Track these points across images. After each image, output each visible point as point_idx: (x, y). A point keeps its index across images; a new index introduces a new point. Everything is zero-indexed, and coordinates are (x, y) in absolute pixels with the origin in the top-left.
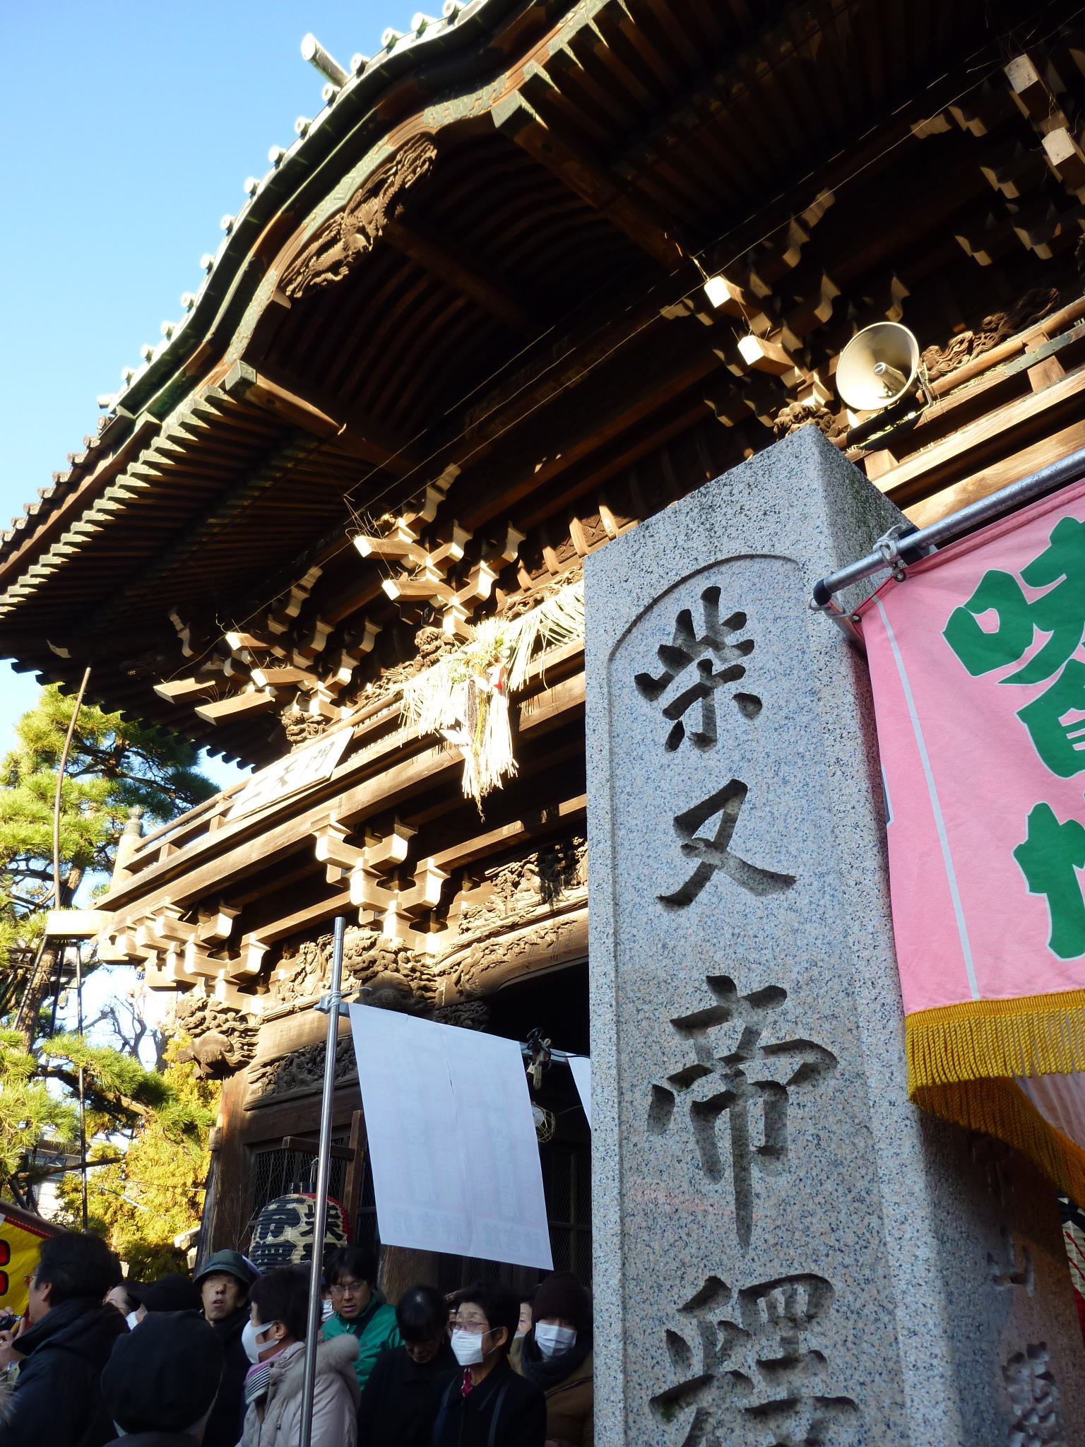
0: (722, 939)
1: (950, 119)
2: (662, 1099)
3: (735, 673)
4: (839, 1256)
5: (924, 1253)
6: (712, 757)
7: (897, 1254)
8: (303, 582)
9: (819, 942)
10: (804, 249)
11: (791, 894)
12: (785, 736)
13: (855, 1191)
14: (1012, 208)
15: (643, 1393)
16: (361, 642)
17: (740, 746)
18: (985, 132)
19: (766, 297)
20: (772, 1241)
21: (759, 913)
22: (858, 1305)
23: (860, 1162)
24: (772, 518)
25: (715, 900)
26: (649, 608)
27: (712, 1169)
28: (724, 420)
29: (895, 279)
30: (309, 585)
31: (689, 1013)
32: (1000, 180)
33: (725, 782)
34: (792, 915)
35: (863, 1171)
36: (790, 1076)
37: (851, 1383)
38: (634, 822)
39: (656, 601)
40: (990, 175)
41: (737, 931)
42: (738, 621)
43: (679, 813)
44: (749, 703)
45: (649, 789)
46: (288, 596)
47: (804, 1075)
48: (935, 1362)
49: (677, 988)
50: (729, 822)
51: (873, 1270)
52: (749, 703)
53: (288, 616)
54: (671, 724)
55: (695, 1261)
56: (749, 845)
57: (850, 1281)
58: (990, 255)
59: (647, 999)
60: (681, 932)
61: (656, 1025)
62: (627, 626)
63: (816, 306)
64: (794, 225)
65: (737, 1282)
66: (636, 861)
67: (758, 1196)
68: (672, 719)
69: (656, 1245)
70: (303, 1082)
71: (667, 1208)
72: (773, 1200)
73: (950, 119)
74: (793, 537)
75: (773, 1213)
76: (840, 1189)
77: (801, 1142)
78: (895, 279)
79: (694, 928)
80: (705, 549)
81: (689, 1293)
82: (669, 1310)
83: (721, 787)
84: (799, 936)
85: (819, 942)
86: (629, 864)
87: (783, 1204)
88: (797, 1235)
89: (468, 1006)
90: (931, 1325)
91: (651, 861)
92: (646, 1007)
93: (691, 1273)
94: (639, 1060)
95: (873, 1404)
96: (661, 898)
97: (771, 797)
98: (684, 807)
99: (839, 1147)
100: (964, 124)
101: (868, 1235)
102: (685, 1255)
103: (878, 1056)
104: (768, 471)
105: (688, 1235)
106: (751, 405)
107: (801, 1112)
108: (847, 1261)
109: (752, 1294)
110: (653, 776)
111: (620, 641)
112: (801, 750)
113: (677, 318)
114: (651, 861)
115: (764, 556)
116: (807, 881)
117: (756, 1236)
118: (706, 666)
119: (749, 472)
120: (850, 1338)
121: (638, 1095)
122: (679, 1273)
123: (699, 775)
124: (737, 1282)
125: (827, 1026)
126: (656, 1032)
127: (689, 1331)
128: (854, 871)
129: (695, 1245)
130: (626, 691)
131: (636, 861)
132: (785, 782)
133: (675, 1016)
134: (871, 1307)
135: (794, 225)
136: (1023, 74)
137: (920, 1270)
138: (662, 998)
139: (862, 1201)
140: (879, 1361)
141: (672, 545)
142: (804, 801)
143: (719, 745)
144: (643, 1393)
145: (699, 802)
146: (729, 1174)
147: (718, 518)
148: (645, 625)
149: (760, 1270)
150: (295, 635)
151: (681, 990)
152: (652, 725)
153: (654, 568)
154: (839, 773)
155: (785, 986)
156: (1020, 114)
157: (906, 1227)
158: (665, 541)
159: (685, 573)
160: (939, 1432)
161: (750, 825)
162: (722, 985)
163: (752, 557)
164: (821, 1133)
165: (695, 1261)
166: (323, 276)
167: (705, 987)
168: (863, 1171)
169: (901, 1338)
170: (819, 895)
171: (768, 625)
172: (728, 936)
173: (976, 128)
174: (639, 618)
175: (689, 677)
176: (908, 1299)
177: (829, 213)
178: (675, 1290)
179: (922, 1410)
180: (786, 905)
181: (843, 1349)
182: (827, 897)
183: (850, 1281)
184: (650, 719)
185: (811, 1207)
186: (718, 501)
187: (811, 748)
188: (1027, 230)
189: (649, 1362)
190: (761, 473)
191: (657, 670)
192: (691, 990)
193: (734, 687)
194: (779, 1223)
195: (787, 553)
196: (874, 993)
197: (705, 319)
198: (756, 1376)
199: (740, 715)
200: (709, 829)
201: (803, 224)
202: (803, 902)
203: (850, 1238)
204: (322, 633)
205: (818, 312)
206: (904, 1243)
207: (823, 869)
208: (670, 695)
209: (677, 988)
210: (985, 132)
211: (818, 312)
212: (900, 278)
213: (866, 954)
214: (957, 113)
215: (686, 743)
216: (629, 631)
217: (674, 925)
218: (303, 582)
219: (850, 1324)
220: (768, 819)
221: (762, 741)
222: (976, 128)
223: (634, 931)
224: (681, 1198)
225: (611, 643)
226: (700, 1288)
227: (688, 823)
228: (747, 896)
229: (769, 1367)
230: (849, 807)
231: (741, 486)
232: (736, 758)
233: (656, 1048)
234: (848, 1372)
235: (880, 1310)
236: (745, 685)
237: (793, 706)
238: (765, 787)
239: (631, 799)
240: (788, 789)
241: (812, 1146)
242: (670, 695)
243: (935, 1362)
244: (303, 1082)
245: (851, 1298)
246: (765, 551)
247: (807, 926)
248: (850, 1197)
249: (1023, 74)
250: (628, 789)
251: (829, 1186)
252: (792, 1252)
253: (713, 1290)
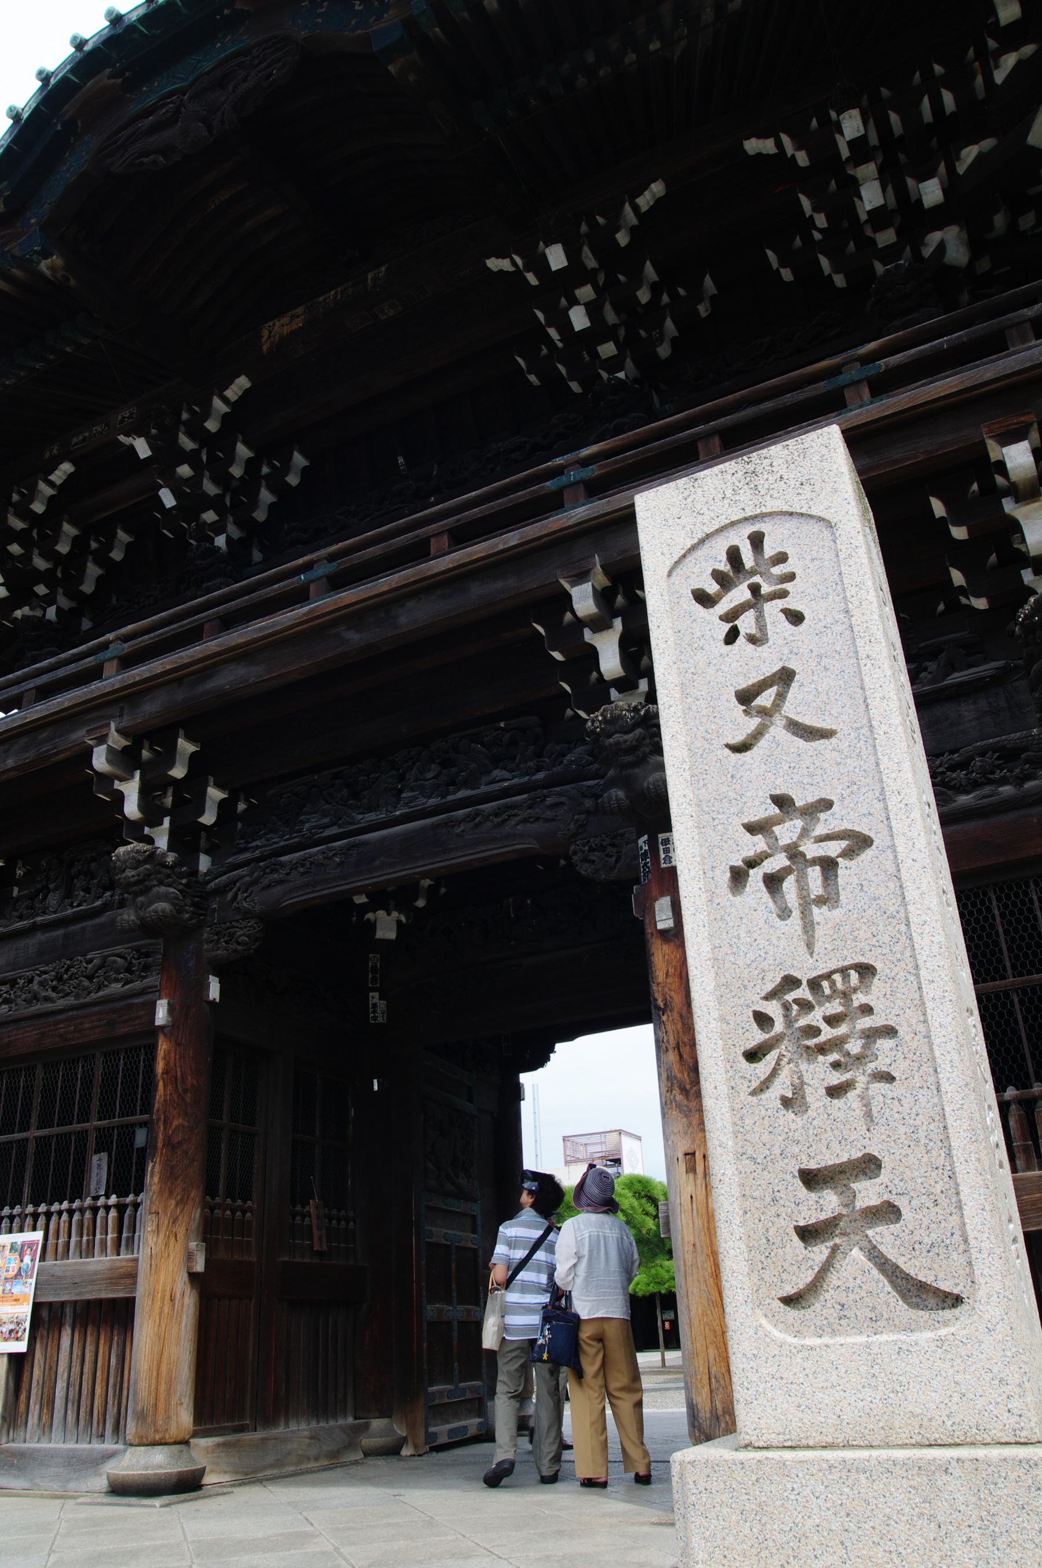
0: (781, 771)
1: (779, 144)
2: (738, 877)
3: (783, 594)
4: (879, 950)
5: (940, 938)
6: (763, 650)
7: (920, 942)
8: (52, 477)
9: (857, 770)
10: (633, 231)
11: (833, 740)
12: (825, 639)
13: (888, 913)
14: (817, 236)
15: (737, 1050)
16: (111, 550)
17: (783, 646)
18: (808, 164)
19: (593, 269)
20: (830, 948)
21: (810, 753)
22: (893, 974)
23: (892, 896)
24: (807, 488)
25: (774, 745)
26: (702, 541)
27: (784, 913)
28: (532, 378)
29: (648, 262)
30: (59, 482)
31: (757, 818)
32: (816, 209)
33: (776, 668)
34: (835, 753)
35: (894, 901)
36: (839, 851)
37: (890, 1016)
38: (699, 693)
39: (708, 536)
40: (805, 202)
41: (792, 765)
42: (781, 558)
43: (740, 688)
44: (795, 618)
45: (711, 670)
46: (33, 489)
47: (848, 854)
48: (946, 994)
49: (745, 803)
50: (781, 697)
51: (902, 953)
52: (795, 618)
53: (32, 511)
54: (727, 627)
55: (772, 967)
56: (799, 710)
57: (887, 962)
58: (794, 273)
59: (721, 811)
60: (746, 767)
61: (730, 828)
62: (683, 552)
63: (639, 289)
64: (627, 208)
65: (804, 976)
66: (704, 720)
67: (818, 924)
68: (728, 622)
69: (740, 963)
70: (47, 999)
71: (748, 939)
72: (830, 925)
73: (779, 144)
74: (826, 504)
75: (831, 932)
76: (878, 913)
77: (849, 888)
78: (648, 262)
79: (758, 763)
80: (751, 503)
81: (770, 987)
82: (754, 999)
83: (774, 670)
84: (841, 766)
85: (857, 770)
86: (697, 722)
87: (837, 927)
88: (849, 942)
89: (244, 924)
90: (943, 976)
91: (717, 720)
92: (720, 816)
93: (769, 976)
94: (716, 851)
95: (905, 1024)
96: (728, 746)
97: (815, 678)
98: (743, 684)
99: (877, 889)
100: (790, 150)
101: (898, 936)
102: (765, 965)
103: (904, 834)
104: (804, 453)
105: (766, 953)
106: (562, 369)
107: (848, 872)
108: (884, 951)
109: (814, 985)
110: (714, 661)
111: (677, 563)
112: (838, 649)
113: (501, 271)
114: (717, 720)
115: (802, 514)
116: (846, 733)
117: (818, 947)
118: (755, 589)
119: (786, 452)
120: (889, 993)
121: (718, 872)
122: (760, 976)
123: (751, 664)
124: (804, 976)
125: (865, 820)
126: (730, 832)
127: (773, 1008)
128: (883, 726)
129: (771, 958)
130: (683, 600)
131: (704, 720)
132: (826, 669)
133: (746, 821)
134: (902, 974)
135: (627, 208)
136: (852, 125)
137: (935, 949)
138: (734, 810)
139: (894, 917)
140: (909, 1001)
141: (721, 496)
142: (841, 682)
143: (770, 643)
144: (737, 1050)
145: (756, 680)
146: (796, 913)
147: (760, 481)
148: (699, 553)
149: (822, 966)
150: (35, 534)
151: (749, 804)
152: (710, 626)
153: (705, 510)
154: (869, 665)
155: (833, 798)
156: (839, 155)
157: (926, 927)
158: (713, 492)
159: (735, 518)
160: (950, 1029)
161: (800, 697)
162: (782, 802)
163: (791, 514)
164: (864, 883)
165: (772, 967)
166: (152, 157)
167: (769, 801)
168: (894, 901)
169: (923, 986)
170: (855, 741)
171: (807, 562)
172: (786, 767)
173: (802, 159)
174: (693, 548)
175: (741, 594)
176: (928, 965)
177: (659, 202)
178: (758, 986)
179: (939, 1020)
180: (830, 747)
181: (883, 1000)
182: (862, 742)
183: (887, 962)
184: (711, 622)
185: (857, 925)
186: (759, 469)
187: (846, 648)
188: (829, 259)
189: (740, 1031)
190: (796, 454)
191: (712, 588)
192: (757, 804)
193: (780, 604)
194: (835, 937)
195: (822, 515)
196: (900, 798)
197: (532, 279)
198: (823, 1026)
199: (787, 623)
200: (766, 699)
201: (636, 208)
202: (844, 745)
203: (886, 939)
204: (67, 535)
205: (639, 293)
206: (924, 935)
207: (859, 725)
208: (725, 605)
209: (745, 803)
210: (808, 164)
211: (639, 293)
212: (711, 276)
213: (894, 775)
214: (786, 139)
215: (741, 640)
216: (684, 556)
217: (740, 763)
218: (52, 477)
219: (888, 985)
220: (814, 692)
221: (806, 642)
222: (802, 159)
223: (707, 767)
224: (759, 932)
225: (669, 564)
226: (776, 983)
227: (745, 697)
228: (801, 742)
229: (832, 1021)
230: (878, 686)
231: (780, 461)
232: (786, 652)
233: (730, 842)
234: (888, 1011)
235: (908, 975)
236: (791, 603)
237: (829, 620)
238: (810, 672)
239: (695, 677)
240: (828, 674)
241: (857, 891)
242: (725, 605)
243: (946, 994)
244: (47, 999)
245: (888, 971)
246: (803, 511)
247: (848, 761)
248: (885, 916)
249: (852, 125)
250: (692, 670)
251: (870, 912)
252: (845, 952)
253: (790, 982)
